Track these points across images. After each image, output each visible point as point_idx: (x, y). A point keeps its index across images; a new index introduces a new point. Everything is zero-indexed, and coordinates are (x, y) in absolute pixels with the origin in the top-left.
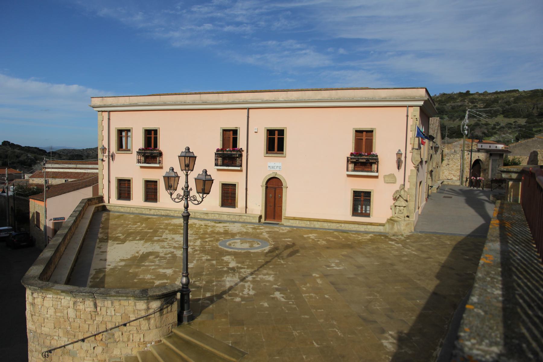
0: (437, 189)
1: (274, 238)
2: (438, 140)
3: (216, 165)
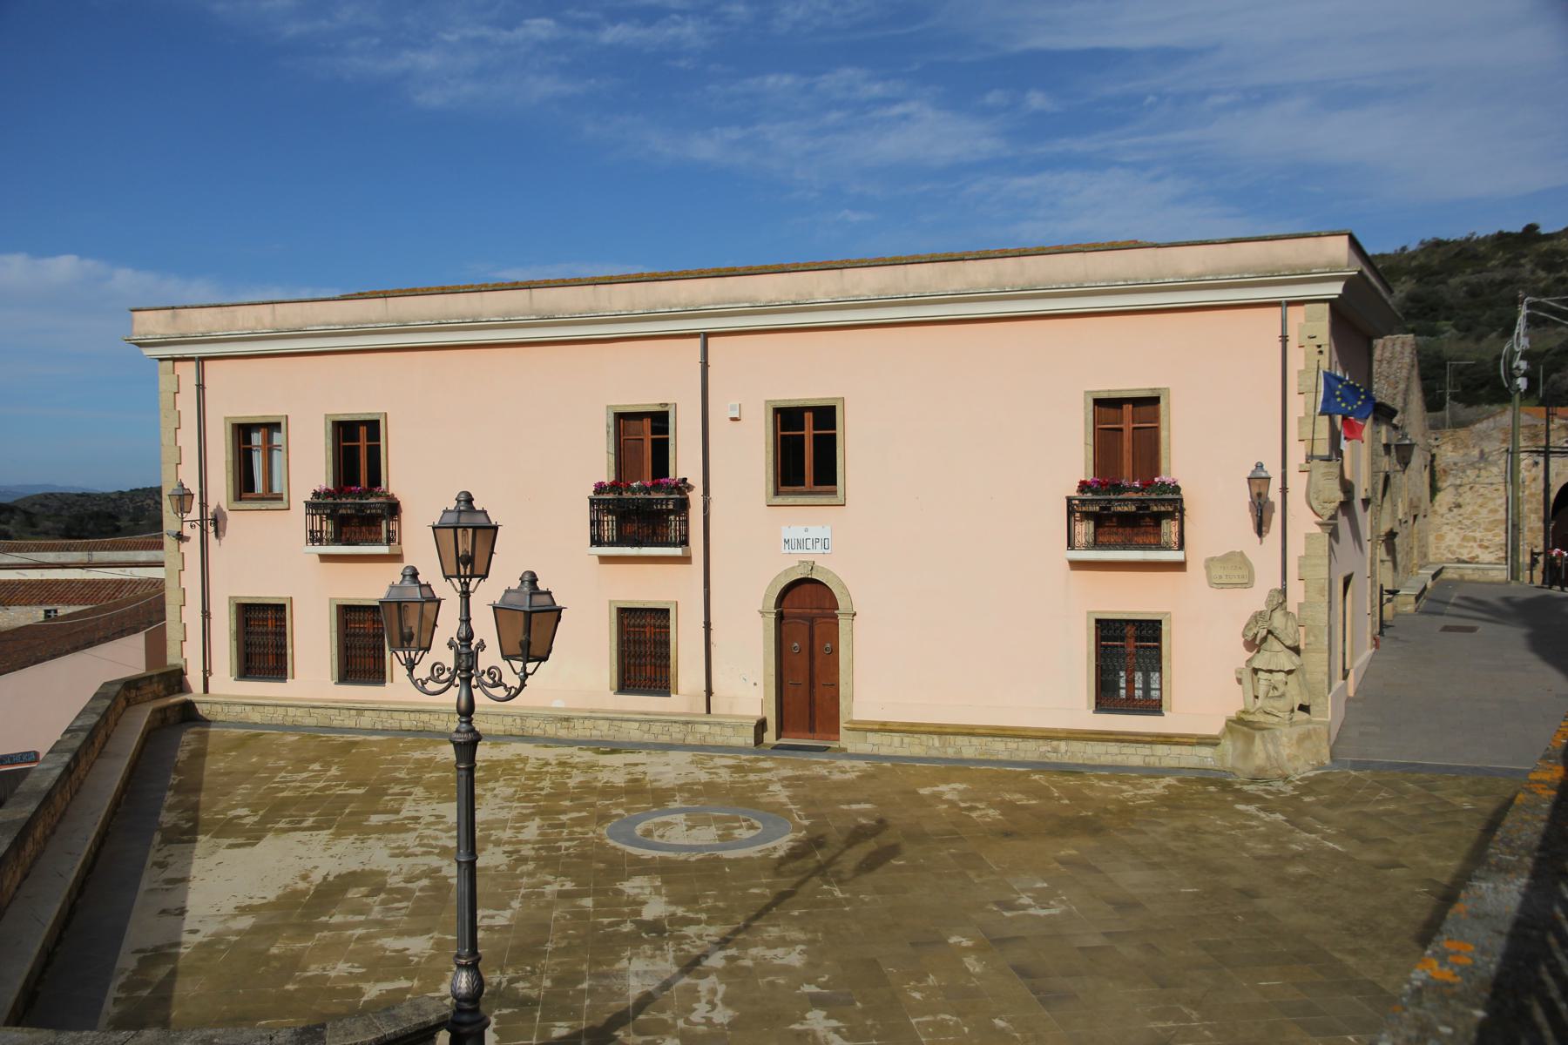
0: (1417, 598)
1: (808, 804)
2: (1414, 416)
3: (596, 541)
